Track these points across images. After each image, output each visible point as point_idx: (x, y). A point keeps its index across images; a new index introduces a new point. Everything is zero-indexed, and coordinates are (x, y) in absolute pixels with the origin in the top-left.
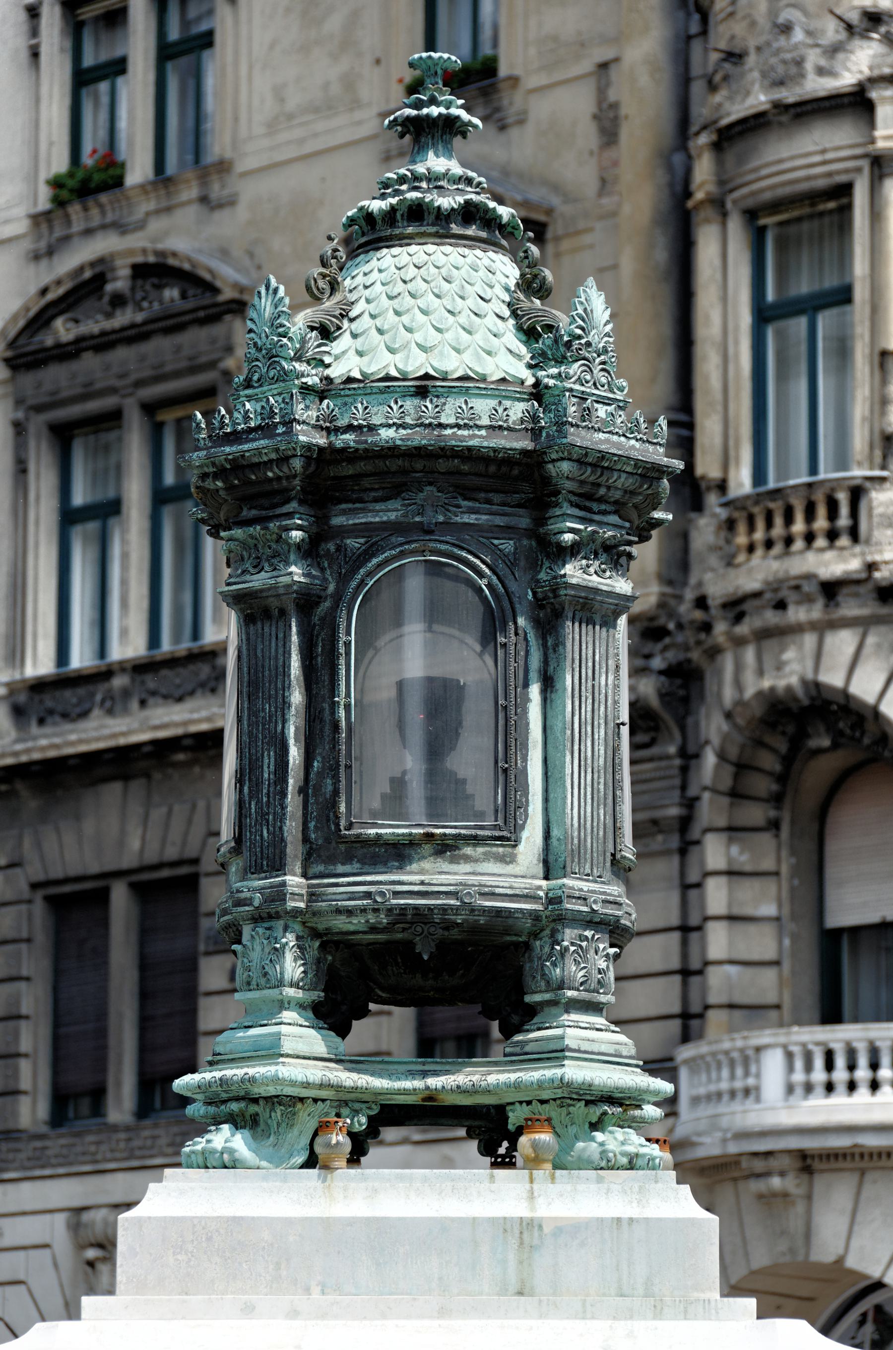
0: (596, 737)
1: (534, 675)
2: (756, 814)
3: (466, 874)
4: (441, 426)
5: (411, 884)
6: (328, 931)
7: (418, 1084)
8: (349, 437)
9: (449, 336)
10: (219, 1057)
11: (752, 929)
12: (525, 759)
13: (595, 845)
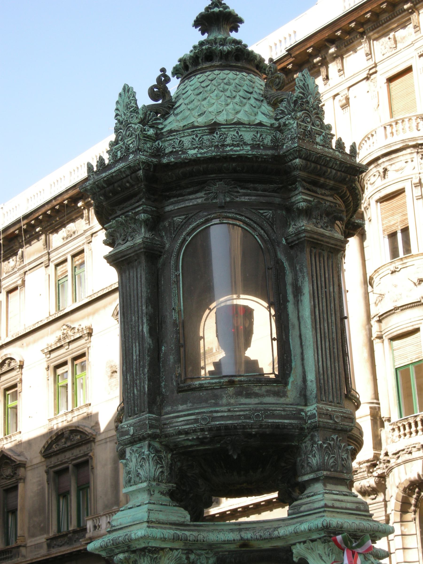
0: (330, 321)
3: (256, 404)
5: (222, 412)
10: (114, 528)
13: (334, 384)
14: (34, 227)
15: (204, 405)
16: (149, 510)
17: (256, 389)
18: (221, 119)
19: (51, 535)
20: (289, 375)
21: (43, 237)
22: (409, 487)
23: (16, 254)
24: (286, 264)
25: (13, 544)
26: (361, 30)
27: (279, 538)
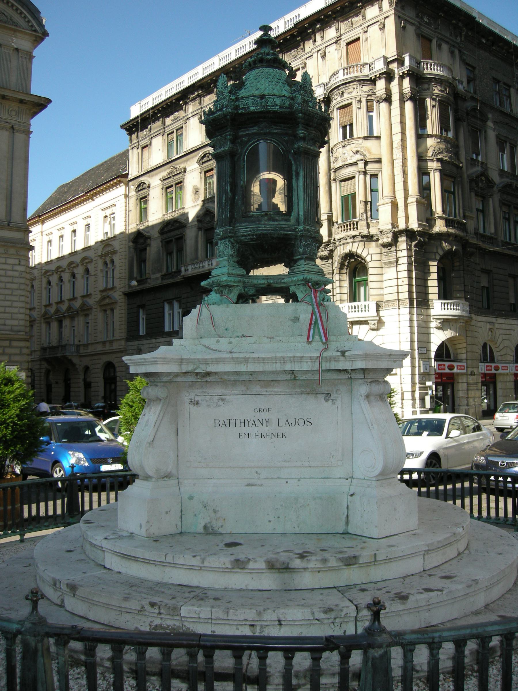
14: (157, 114)
15: (254, 224)
16: (229, 269)
17: (277, 218)
18: (266, 93)
19: (163, 273)
20: (292, 212)
21: (161, 119)
22: (344, 257)
23: (147, 128)
24: (293, 162)
25: (144, 277)
26: (334, 16)
27: (284, 283)
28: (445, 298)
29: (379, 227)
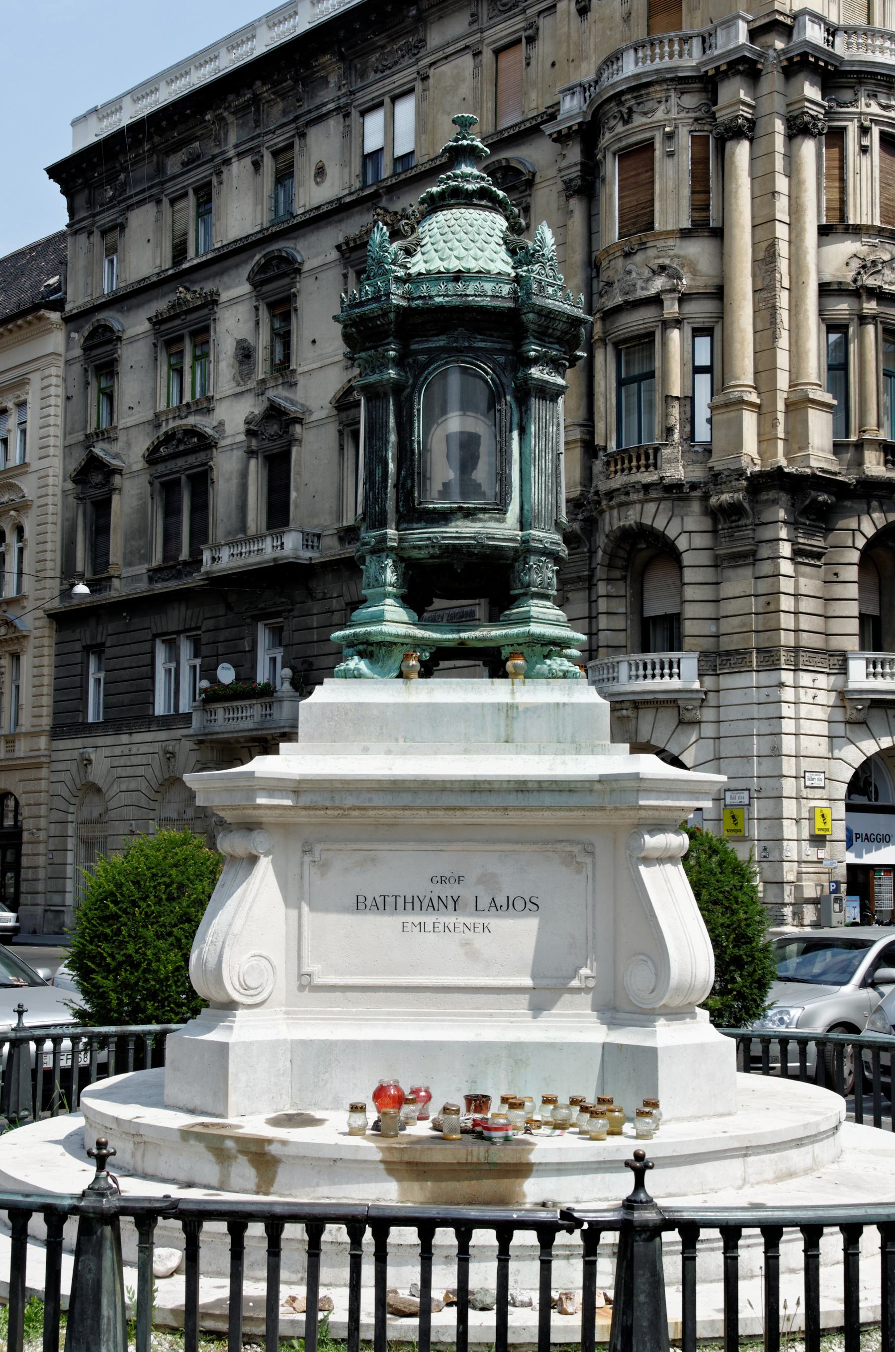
1: (515, 426)
2: (617, 574)
4: (466, 295)
6: (409, 558)
7: (455, 636)
8: (419, 302)
9: (471, 252)
11: (615, 617)
12: (510, 469)
19: (154, 564)
28: (877, 647)
29: (710, 465)
